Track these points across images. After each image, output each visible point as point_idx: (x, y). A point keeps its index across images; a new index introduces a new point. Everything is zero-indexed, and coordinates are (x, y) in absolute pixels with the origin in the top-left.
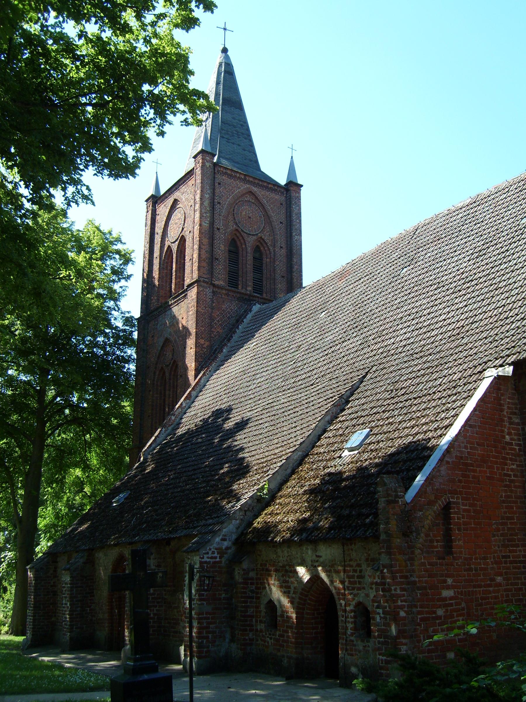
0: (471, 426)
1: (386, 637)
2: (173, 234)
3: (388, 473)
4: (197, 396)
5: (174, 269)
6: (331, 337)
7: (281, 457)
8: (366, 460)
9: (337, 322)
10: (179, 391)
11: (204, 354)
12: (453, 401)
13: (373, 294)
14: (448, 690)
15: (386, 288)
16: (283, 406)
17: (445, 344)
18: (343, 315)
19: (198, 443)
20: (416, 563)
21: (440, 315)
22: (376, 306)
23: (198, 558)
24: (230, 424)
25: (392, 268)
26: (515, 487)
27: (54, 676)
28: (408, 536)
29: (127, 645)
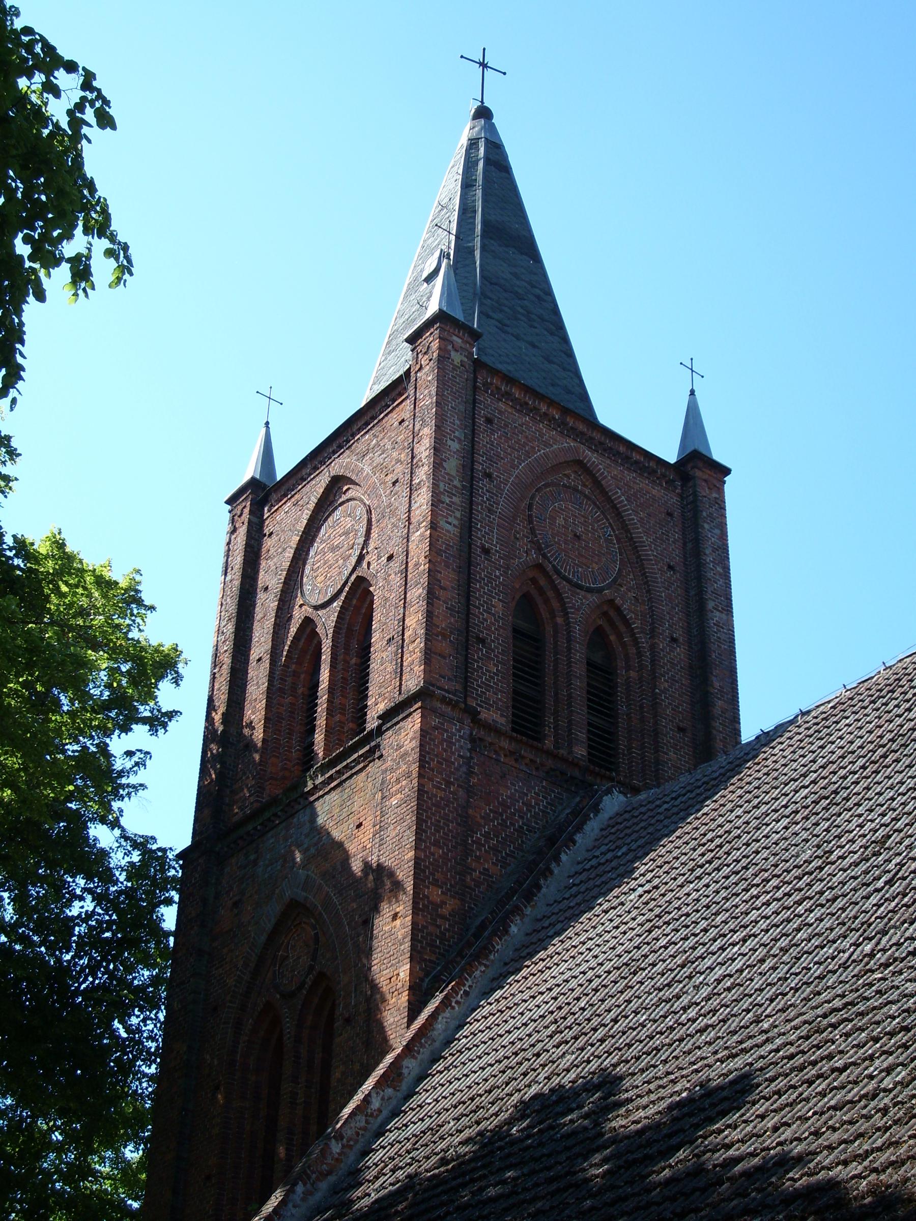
2: (324, 578)
4: (422, 1077)
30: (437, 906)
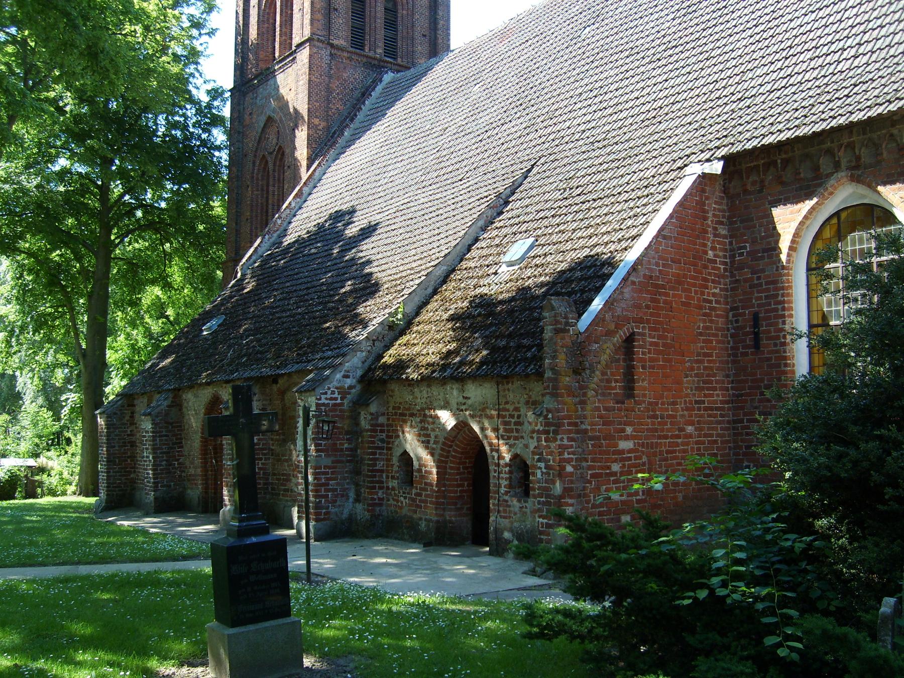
0: (664, 237)
1: (548, 496)
3: (557, 294)
5: (278, 23)
6: (487, 118)
7: (419, 272)
8: (529, 278)
9: (496, 97)
10: (286, 187)
11: (319, 138)
12: (643, 205)
13: (545, 62)
14: (624, 556)
15: (561, 53)
16: (423, 206)
17: (636, 130)
18: (503, 88)
19: (311, 254)
20: (589, 407)
21: (632, 92)
22: (548, 77)
23: (314, 398)
24: (354, 230)
25: (571, 26)
26: (717, 316)
27: (137, 543)
28: (580, 374)
29: (226, 505)
30: (317, 126)
